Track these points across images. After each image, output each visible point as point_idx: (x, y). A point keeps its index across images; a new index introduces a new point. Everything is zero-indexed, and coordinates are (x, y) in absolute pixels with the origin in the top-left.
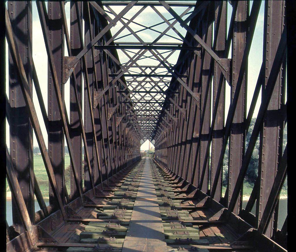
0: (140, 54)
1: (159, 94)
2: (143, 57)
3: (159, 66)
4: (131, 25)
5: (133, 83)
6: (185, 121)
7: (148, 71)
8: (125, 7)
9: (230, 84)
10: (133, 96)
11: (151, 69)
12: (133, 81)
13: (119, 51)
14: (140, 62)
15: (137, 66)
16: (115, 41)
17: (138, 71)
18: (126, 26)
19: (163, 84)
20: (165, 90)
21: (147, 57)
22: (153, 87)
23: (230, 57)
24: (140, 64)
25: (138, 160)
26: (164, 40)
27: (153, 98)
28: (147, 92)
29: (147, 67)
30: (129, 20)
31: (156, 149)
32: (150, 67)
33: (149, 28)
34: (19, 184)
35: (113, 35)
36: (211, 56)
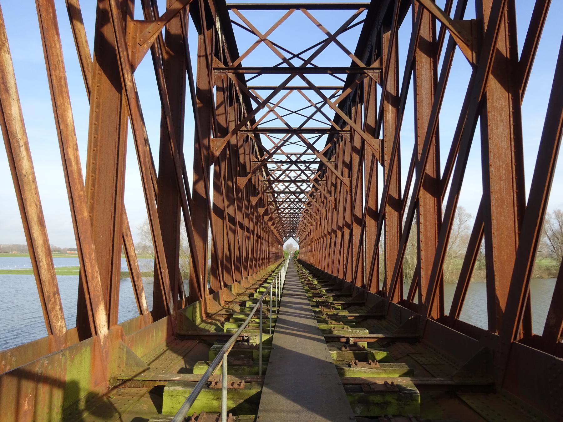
0: (285, 140)
1: (305, 184)
2: (287, 143)
3: (304, 153)
4: (277, 109)
5: (276, 172)
6: (334, 210)
7: (294, 158)
8: (273, 91)
9: (383, 165)
10: (276, 186)
11: (296, 156)
12: (277, 170)
13: (262, 136)
14: (285, 149)
15: (283, 153)
16: (258, 127)
17: (283, 158)
18: (271, 110)
19: (310, 172)
20: (312, 177)
21: (292, 143)
22: (294, 206)
23: (381, 137)
24: (286, 151)
25: (278, 257)
26: (311, 125)
27: (295, 211)
28: (291, 181)
29: (292, 154)
30: (277, 107)
31: (301, 248)
32: (295, 154)
33: (295, 112)
34: (338, 126)
35: (257, 120)
36: (361, 137)
